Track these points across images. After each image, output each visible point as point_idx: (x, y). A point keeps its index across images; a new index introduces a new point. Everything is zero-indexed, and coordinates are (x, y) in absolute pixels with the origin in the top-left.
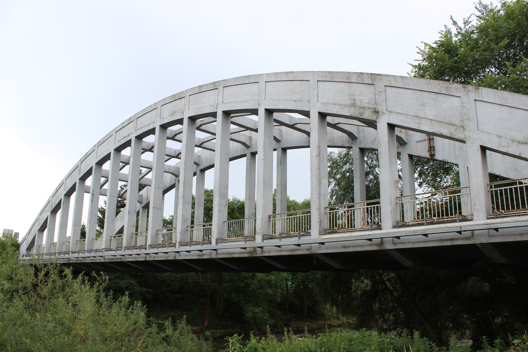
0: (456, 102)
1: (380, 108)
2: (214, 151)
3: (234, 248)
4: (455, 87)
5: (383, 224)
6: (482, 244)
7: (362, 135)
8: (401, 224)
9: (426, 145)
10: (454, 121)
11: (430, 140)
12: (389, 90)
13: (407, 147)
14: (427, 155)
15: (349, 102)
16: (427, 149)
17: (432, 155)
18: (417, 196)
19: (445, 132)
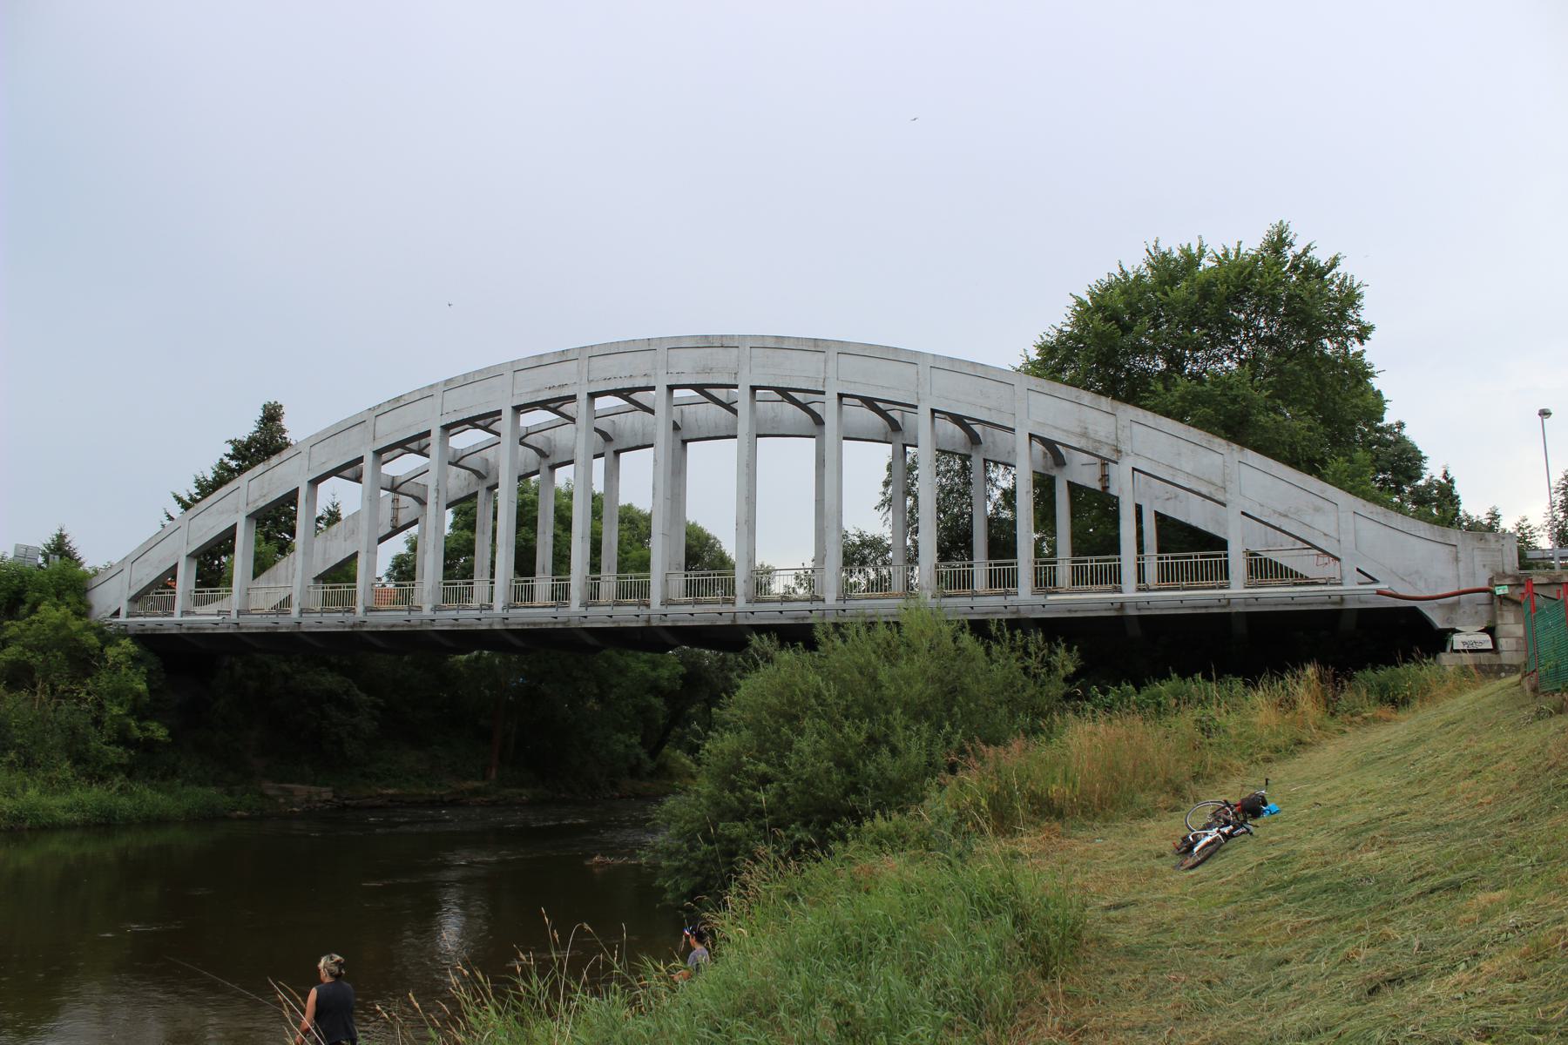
0: (1217, 459)
1: (1123, 447)
2: (652, 412)
3: (627, 615)
4: (1219, 443)
5: (1123, 586)
6: (1238, 614)
7: (990, 439)
8: (667, 602)
9: (1096, 471)
10: (1214, 479)
11: (1103, 465)
12: (1135, 426)
13: (1066, 470)
14: (1098, 486)
15: (1078, 430)
16: (1099, 476)
17: (1105, 488)
18: (1536, 590)
19: (1204, 491)
